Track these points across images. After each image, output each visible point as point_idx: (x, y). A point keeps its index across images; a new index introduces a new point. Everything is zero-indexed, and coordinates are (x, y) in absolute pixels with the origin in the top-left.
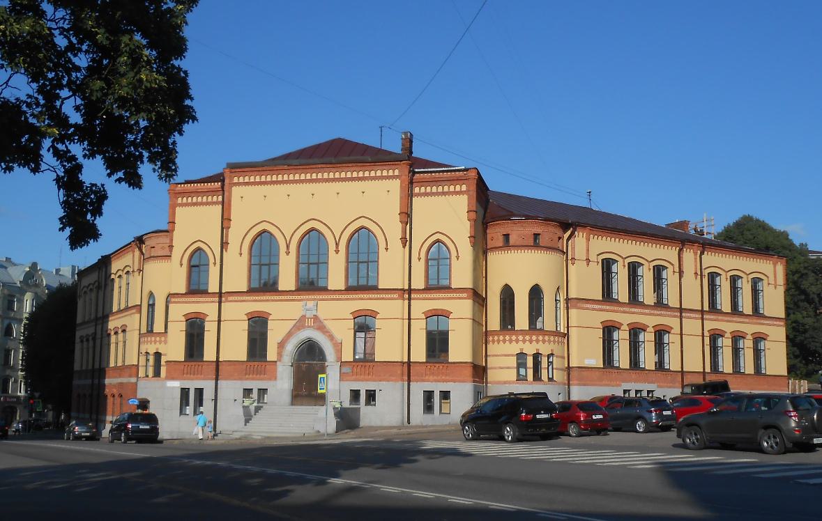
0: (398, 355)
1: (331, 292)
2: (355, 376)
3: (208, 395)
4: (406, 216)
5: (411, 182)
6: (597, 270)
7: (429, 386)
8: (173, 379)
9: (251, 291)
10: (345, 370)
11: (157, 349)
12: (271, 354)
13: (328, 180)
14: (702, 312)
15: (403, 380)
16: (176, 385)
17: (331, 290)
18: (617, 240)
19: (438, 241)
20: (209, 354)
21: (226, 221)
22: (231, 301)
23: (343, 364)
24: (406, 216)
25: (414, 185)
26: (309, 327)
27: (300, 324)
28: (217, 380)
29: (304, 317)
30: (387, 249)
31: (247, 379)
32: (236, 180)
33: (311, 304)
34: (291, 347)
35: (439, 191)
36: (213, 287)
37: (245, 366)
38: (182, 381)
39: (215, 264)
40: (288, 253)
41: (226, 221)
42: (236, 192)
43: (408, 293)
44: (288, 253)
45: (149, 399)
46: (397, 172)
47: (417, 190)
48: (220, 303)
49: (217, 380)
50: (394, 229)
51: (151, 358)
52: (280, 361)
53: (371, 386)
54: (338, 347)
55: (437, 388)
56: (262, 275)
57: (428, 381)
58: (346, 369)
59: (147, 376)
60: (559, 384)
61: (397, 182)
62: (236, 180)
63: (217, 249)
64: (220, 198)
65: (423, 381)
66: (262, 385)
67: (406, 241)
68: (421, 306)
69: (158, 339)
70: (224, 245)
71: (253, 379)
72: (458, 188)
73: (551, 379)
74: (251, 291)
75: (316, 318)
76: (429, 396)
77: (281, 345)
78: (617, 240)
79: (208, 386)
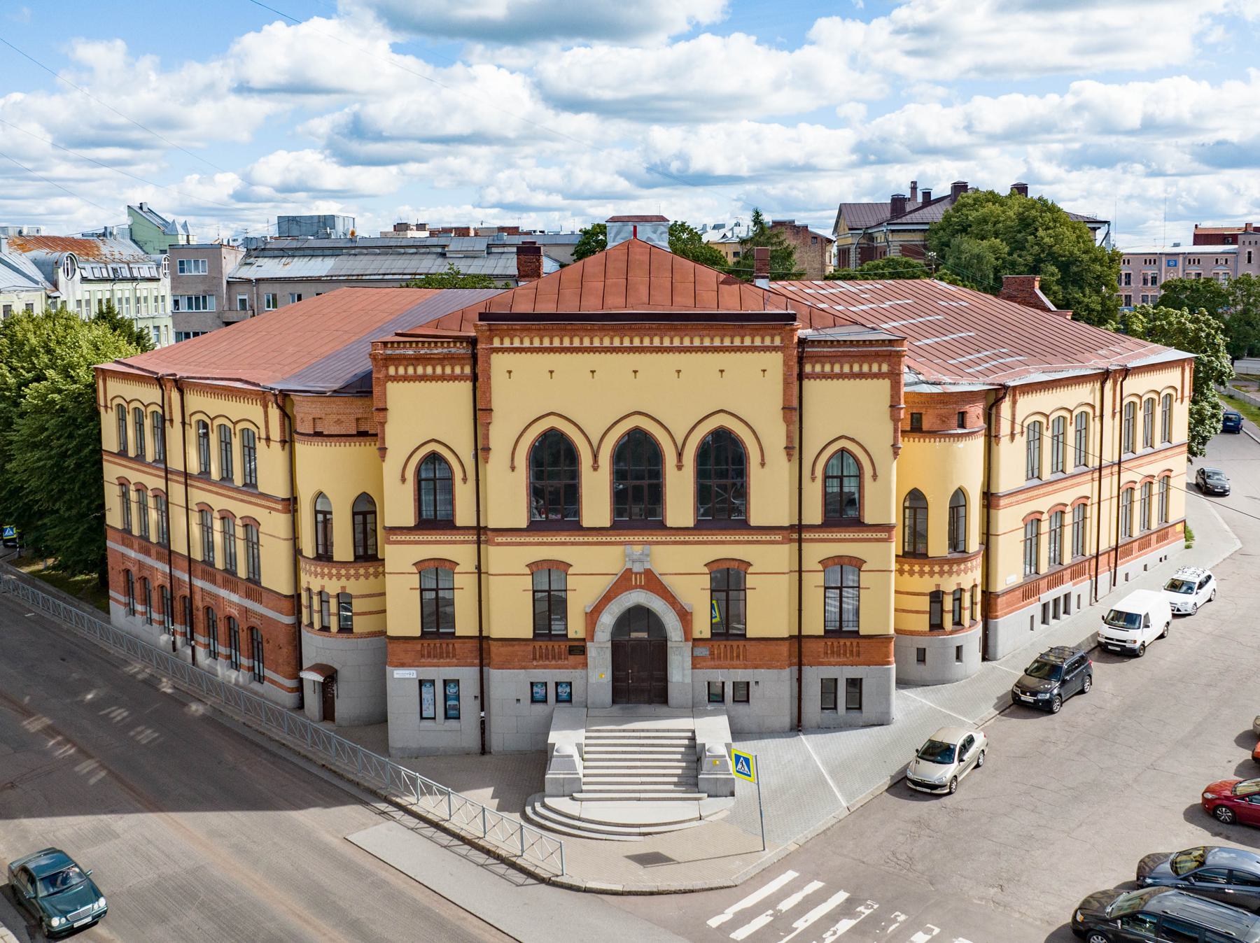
0: (781, 627)
1: (673, 532)
2: (716, 660)
3: (469, 689)
4: (794, 411)
5: (801, 361)
6: (312, 422)
7: (829, 672)
8: (402, 665)
9: (533, 527)
10: (698, 652)
11: (343, 588)
12: (576, 627)
13: (705, 350)
14: (799, 528)
15: (790, 665)
16: (410, 674)
17: (671, 528)
18: (932, 440)
19: (843, 451)
20: (465, 625)
21: (481, 412)
22: (499, 544)
23: (696, 641)
24: (794, 411)
25: (805, 361)
26: (636, 587)
27: (624, 582)
28: (481, 666)
29: (629, 571)
30: (763, 464)
31: (536, 667)
32: (496, 343)
33: (638, 549)
34: (608, 619)
35: (665, 345)
36: (464, 515)
37: (530, 648)
38: (420, 669)
39: (465, 480)
40: (595, 467)
41: (481, 412)
42: (499, 363)
43: (797, 532)
44: (595, 467)
45: (336, 666)
46: (777, 341)
47: (808, 368)
48: (479, 543)
49: (800, 665)
50: (774, 433)
51: (333, 602)
52: (592, 640)
53: (741, 675)
54: (685, 616)
55: (843, 673)
56: (1114, 556)
57: (830, 664)
58: (703, 651)
59: (325, 629)
60: (362, 636)
61: (778, 357)
62: (496, 343)
63: (467, 454)
64: (468, 370)
65: (821, 664)
66: (563, 675)
67: (794, 448)
68: (816, 552)
69: (343, 572)
70: (481, 450)
71: (545, 667)
72: (875, 368)
73: (346, 629)
74: (533, 527)
75: (648, 573)
76: (829, 687)
77: (592, 616)
78: (932, 440)
79: (467, 676)
